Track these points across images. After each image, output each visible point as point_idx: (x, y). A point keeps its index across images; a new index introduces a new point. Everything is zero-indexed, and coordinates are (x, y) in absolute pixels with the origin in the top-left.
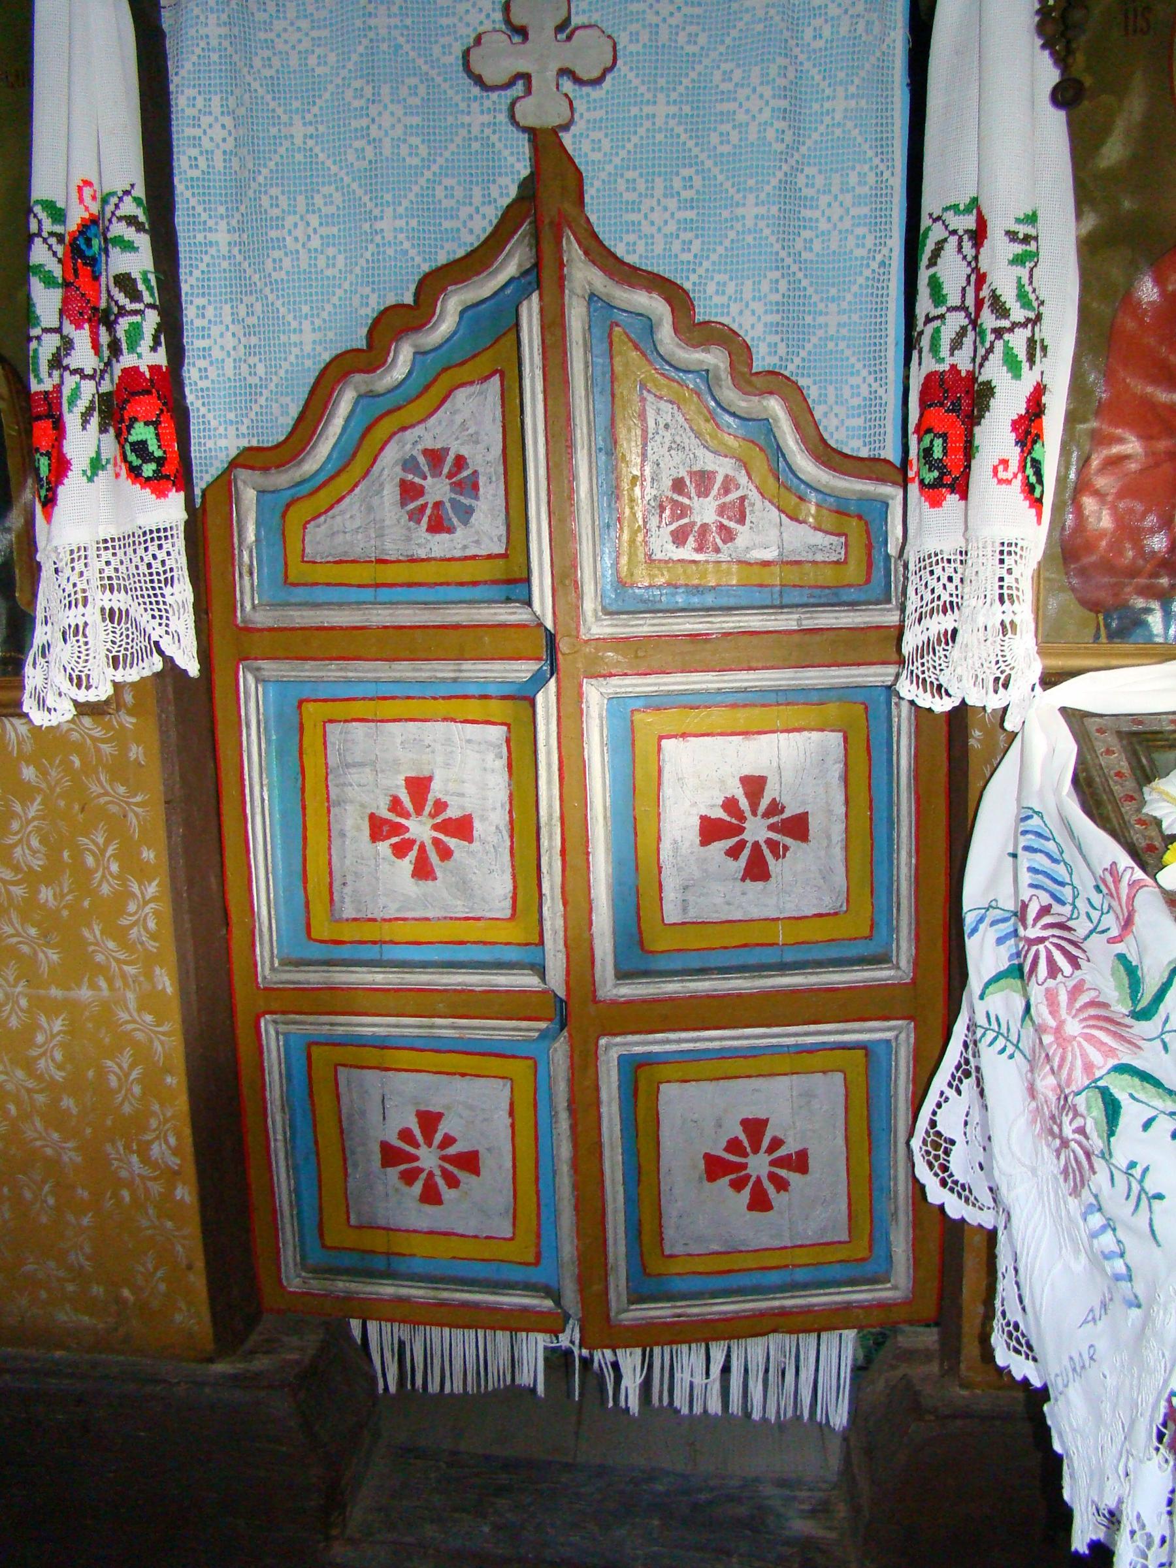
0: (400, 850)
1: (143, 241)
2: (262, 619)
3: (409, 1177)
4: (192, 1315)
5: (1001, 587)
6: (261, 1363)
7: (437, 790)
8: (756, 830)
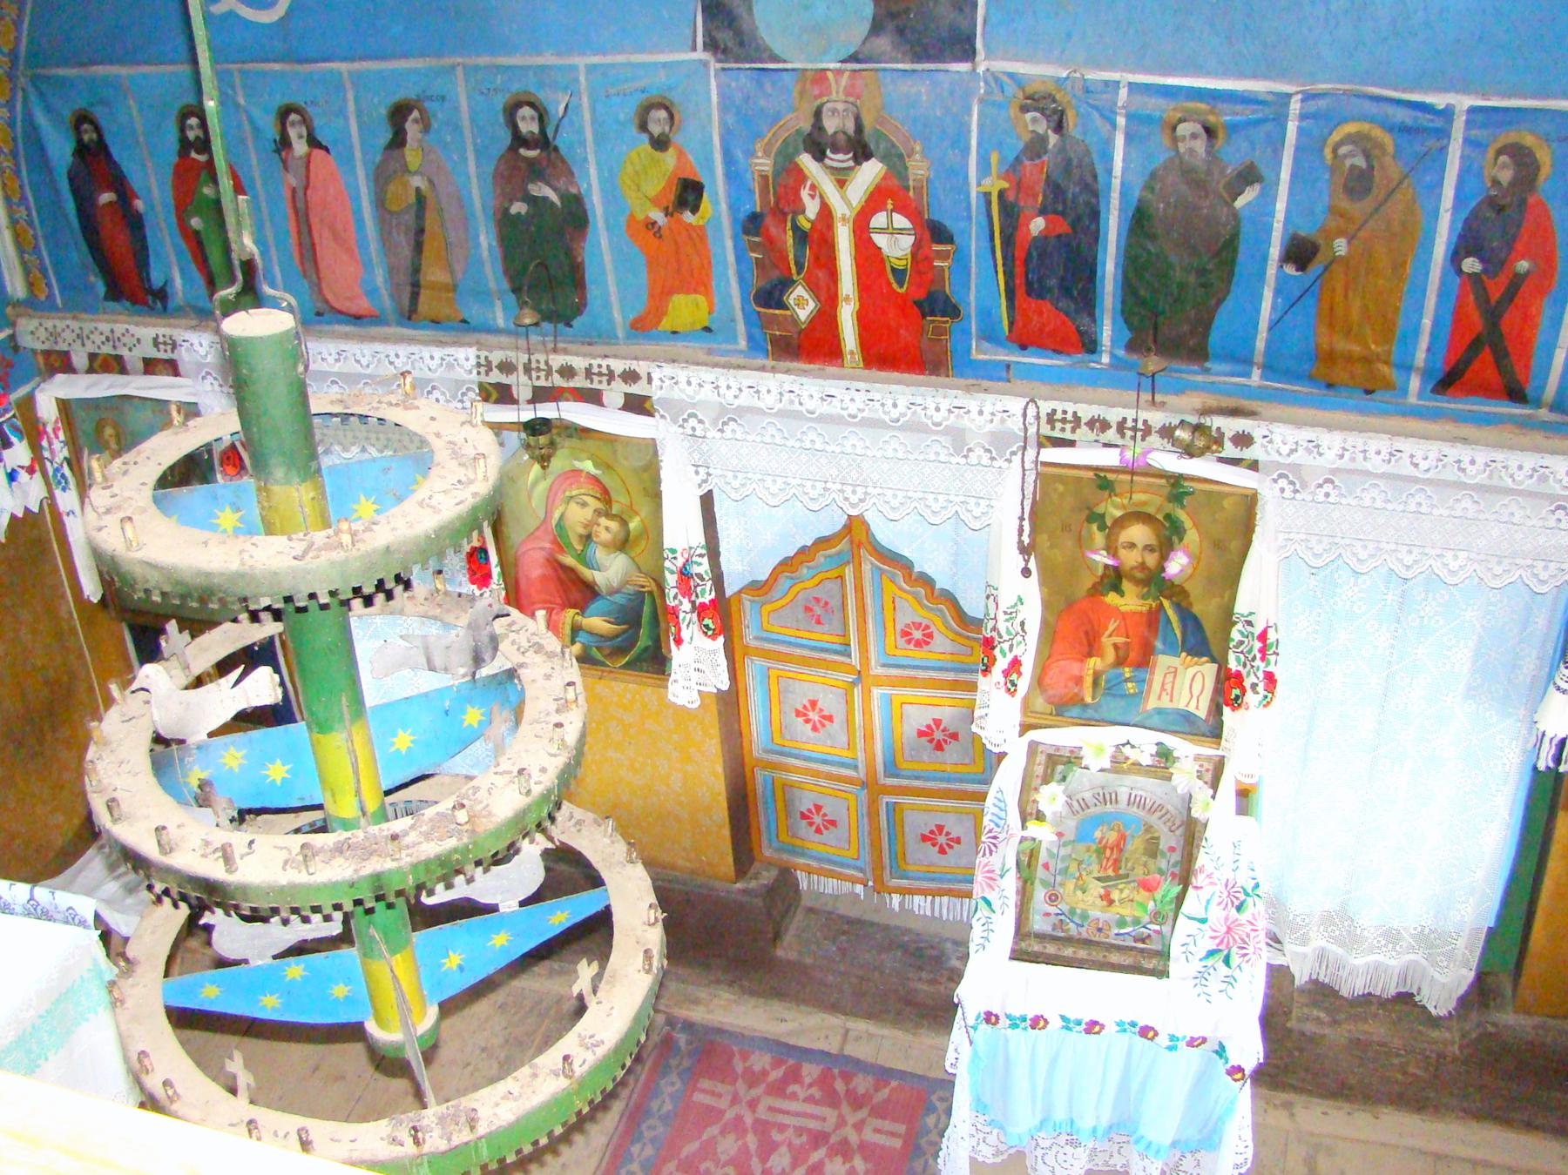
0: (807, 721)
1: (705, 560)
2: (754, 643)
3: (811, 824)
4: (727, 864)
5: (630, 1071)
6: (753, 884)
7: (820, 705)
8: (938, 735)
